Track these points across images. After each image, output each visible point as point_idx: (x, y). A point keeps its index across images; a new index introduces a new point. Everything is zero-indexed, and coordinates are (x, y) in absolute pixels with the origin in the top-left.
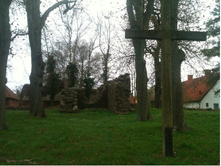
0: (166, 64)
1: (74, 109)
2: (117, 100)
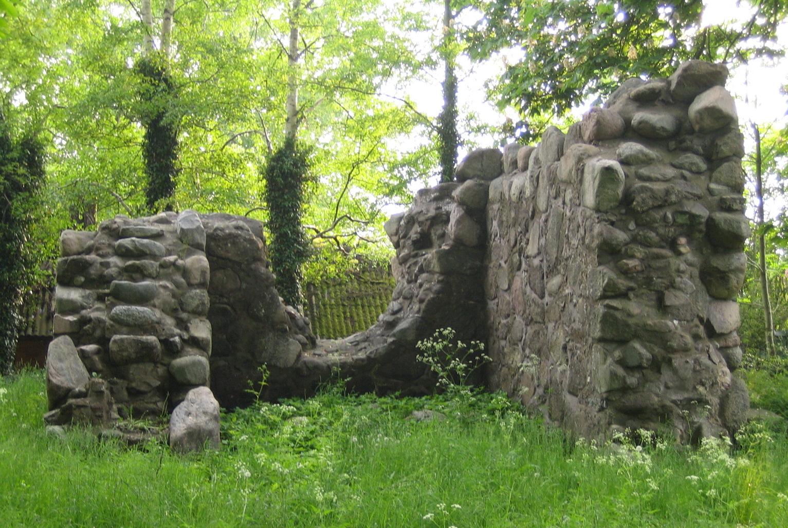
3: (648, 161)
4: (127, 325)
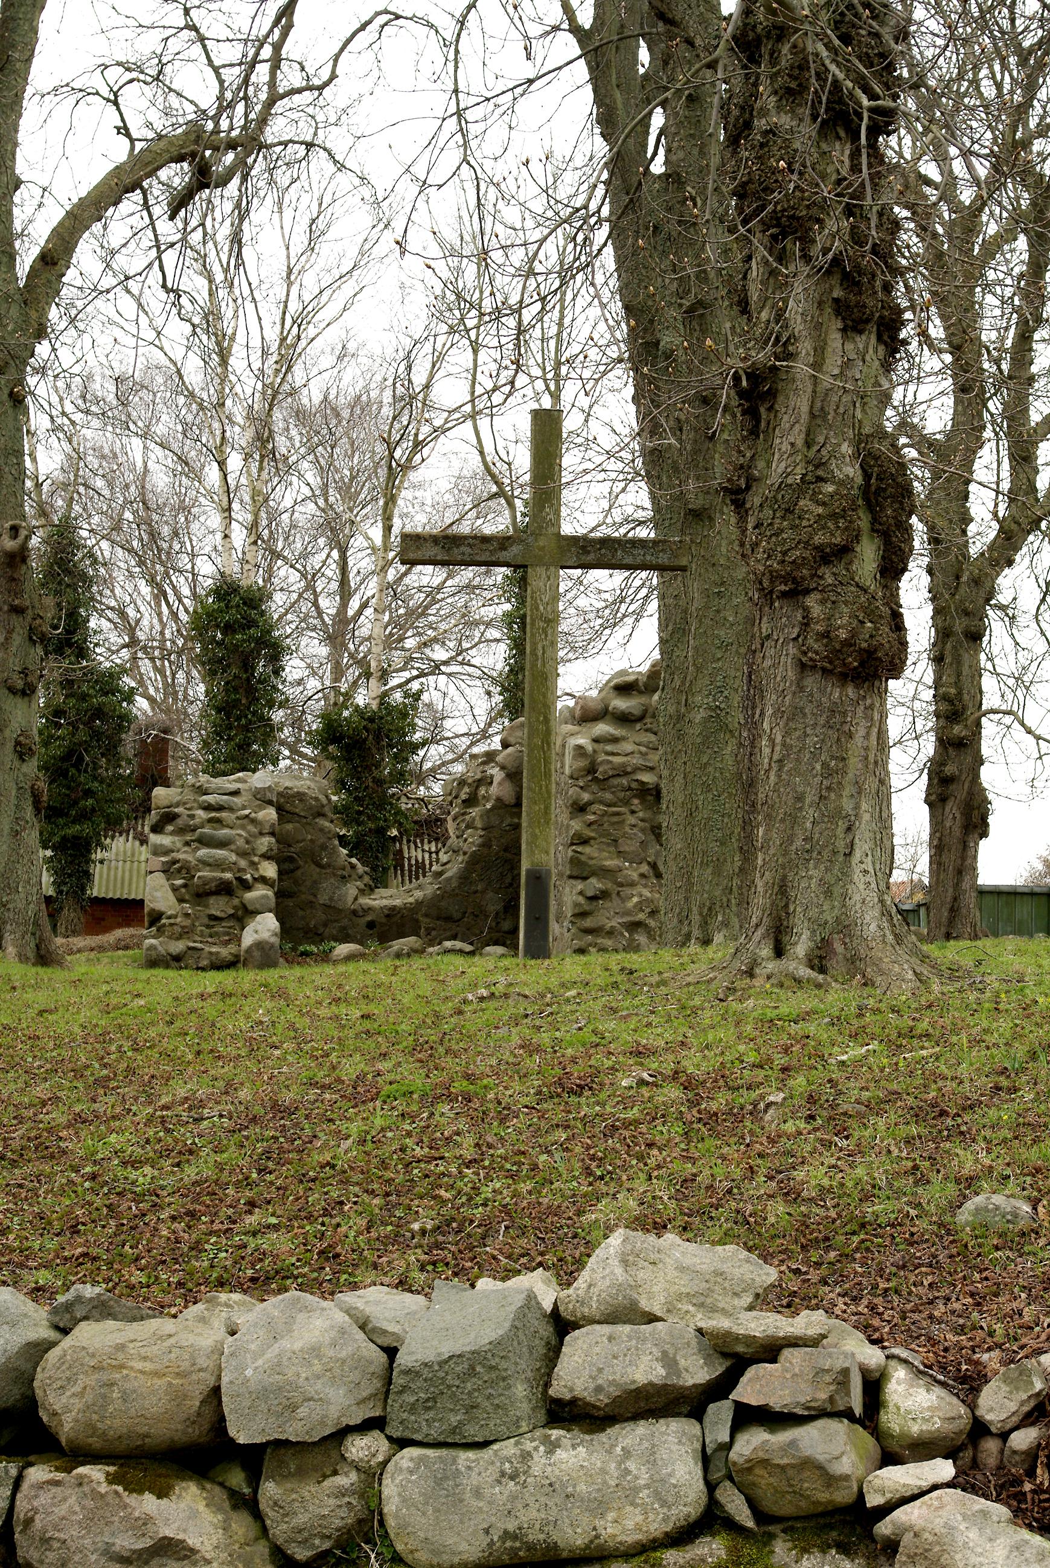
0: (540, 653)
1: (249, 938)
2: (580, 871)
3: (615, 740)
4: (210, 865)
